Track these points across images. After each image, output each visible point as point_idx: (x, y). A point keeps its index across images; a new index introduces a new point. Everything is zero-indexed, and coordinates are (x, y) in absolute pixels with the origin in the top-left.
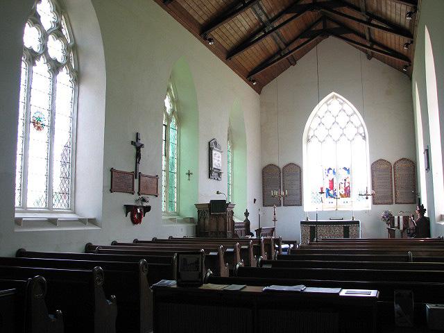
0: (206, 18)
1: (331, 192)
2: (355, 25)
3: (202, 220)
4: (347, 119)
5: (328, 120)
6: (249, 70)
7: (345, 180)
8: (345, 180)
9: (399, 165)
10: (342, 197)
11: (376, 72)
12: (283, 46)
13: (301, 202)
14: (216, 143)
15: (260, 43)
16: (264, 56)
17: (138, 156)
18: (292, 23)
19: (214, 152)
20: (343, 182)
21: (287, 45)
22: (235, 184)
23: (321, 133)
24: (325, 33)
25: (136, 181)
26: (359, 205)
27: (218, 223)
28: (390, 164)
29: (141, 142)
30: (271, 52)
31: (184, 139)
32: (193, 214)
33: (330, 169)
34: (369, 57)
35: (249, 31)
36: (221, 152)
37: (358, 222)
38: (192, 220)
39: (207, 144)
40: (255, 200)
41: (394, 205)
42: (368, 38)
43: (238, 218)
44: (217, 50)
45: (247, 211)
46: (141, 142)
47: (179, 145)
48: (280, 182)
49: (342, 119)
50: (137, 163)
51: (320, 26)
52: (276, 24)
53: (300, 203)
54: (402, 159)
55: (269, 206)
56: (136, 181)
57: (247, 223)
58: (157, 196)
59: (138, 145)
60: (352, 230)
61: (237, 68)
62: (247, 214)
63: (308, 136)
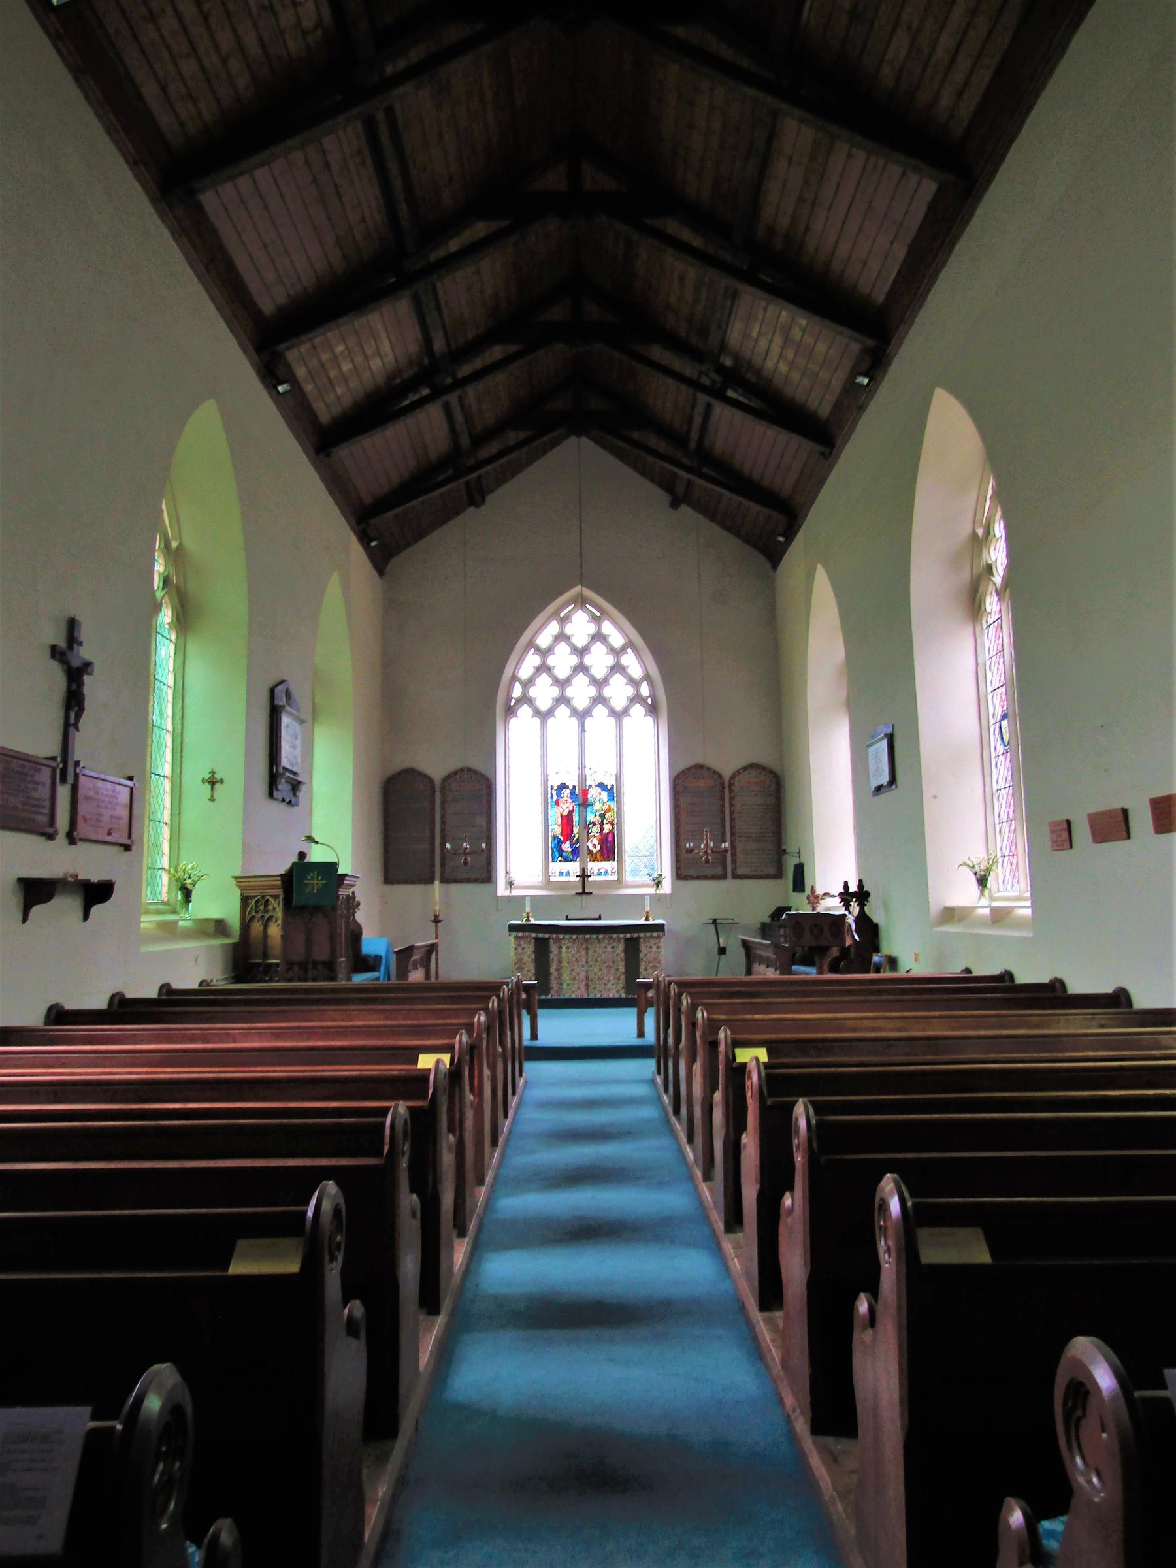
0: (281, 298)
1: (566, 846)
2: (666, 397)
3: (257, 927)
4: (610, 660)
5: (562, 660)
6: (368, 500)
7: (603, 816)
8: (603, 816)
11: (680, 545)
12: (465, 441)
14: (288, 694)
15: (410, 421)
16: (412, 464)
17: (74, 701)
18: (500, 377)
19: (285, 720)
20: (598, 819)
21: (479, 440)
23: (544, 692)
24: (578, 423)
25: (63, 792)
27: (309, 943)
28: (720, 776)
29: (85, 652)
30: (433, 456)
31: (197, 673)
33: (563, 786)
34: (675, 504)
35: (390, 377)
38: (220, 927)
39: (279, 680)
41: (728, 884)
42: (693, 445)
44: (298, 411)
46: (85, 652)
47: (180, 692)
48: (433, 817)
49: (599, 661)
50: (69, 727)
51: (557, 313)
52: (465, 370)
53: (486, 875)
54: (753, 766)
56: (63, 792)
58: (127, 848)
59: (76, 664)
60: (646, 950)
61: (338, 485)
63: (509, 698)
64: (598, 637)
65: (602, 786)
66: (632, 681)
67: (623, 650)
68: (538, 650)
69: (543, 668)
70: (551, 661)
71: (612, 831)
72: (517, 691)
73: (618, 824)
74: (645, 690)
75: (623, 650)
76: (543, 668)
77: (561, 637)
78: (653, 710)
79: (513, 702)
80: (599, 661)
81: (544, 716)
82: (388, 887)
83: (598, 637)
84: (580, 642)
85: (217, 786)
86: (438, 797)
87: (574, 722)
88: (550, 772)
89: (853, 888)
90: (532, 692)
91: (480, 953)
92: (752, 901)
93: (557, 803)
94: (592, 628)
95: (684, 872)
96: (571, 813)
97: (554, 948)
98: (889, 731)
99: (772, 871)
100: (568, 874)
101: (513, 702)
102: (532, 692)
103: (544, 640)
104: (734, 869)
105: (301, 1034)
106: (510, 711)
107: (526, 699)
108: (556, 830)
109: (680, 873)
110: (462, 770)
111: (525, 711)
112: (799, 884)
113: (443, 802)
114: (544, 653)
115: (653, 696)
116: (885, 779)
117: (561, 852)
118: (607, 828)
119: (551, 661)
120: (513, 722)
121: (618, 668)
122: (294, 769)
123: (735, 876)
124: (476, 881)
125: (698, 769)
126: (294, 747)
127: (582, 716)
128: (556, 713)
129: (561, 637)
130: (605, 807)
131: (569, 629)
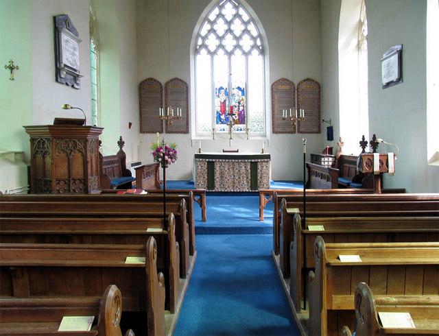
4: (243, 27)
5: (221, 27)
7: (239, 103)
8: (239, 103)
9: (304, 86)
10: (236, 123)
13: (188, 128)
22: (103, 101)
23: (212, 42)
26: (257, 136)
32: (21, 145)
33: (221, 88)
36: (79, 41)
37: (268, 157)
40: (130, 124)
41: (297, 135)
43: (109, 149)
45: (121, 139)
48: (159, 100)
49: (238, 27)
53: (186, 131)
54: (307, 80)
55: (147, 132)
57: (122, 157)
62: (121, 143)
63: (196, 45)
64: (237, 15)
65: (239, 88)
66: (253, 38)
67: (248, 22)
68: (210, 22)
69: (212, 31)
70: (215, 27)
71: (243, 110)
72: (200, 42)
73: (246, 107)
74: (259, 43)
75: (248, 22)
76: (212, 31)
77: (220, 15)
78: (262, 52)
79: (198, 47)
80: (238, 27)
81: (212, 54)
82: (142, 135)
83: (237, 15)
84: (229, 18)
85: (15, 70)
86: (164, 91)
87: (226, 57)
88: (216, 80)
89: (368, 139)
90: (207, 42)
91: (180, 170)
92: (309, 143)
93: (219, 96)
94: (234, 12)
95: (276, 130)
96: (225, 101)
97: (217, 168)
98: (399, 47)
99: (316, 130)
100: (224, 130)
101: (198, 47)
102: (207, 42)
103: (212, 17)
104: (299, 129)
105: (101, 208)
106: (197, 51)
107: (204, 46)
108: (219, 109)
109: (274, 132)
110: (175, 79)
111: (203, 51)
112: (330, 134)
113: (166, 94)
114: (212, 23)
115: (262, 45)
116: (395, 77)
117: (220, 119)
118: (241, 108)
119: (215, 27)
120: (198, 57)
121: (246, 31)
122: (75, 67)
123: (299, 132)
124: (182, 132)
125: (284, 80)
126: (73, 54)
127: (230, 54)
128: (218, 22)
129: (220, 15)
130: (241, 99)
131: (224, 12)
